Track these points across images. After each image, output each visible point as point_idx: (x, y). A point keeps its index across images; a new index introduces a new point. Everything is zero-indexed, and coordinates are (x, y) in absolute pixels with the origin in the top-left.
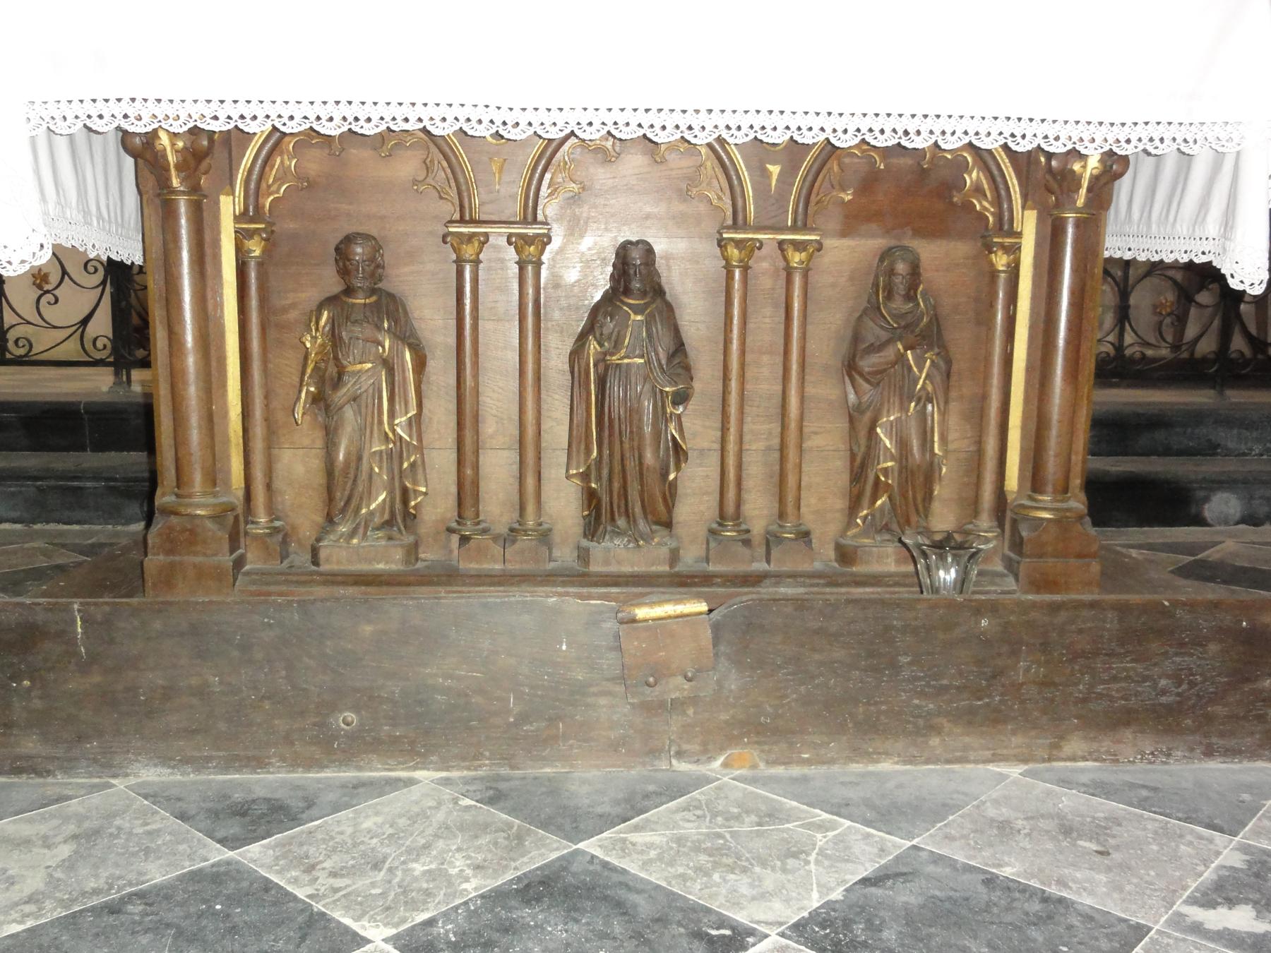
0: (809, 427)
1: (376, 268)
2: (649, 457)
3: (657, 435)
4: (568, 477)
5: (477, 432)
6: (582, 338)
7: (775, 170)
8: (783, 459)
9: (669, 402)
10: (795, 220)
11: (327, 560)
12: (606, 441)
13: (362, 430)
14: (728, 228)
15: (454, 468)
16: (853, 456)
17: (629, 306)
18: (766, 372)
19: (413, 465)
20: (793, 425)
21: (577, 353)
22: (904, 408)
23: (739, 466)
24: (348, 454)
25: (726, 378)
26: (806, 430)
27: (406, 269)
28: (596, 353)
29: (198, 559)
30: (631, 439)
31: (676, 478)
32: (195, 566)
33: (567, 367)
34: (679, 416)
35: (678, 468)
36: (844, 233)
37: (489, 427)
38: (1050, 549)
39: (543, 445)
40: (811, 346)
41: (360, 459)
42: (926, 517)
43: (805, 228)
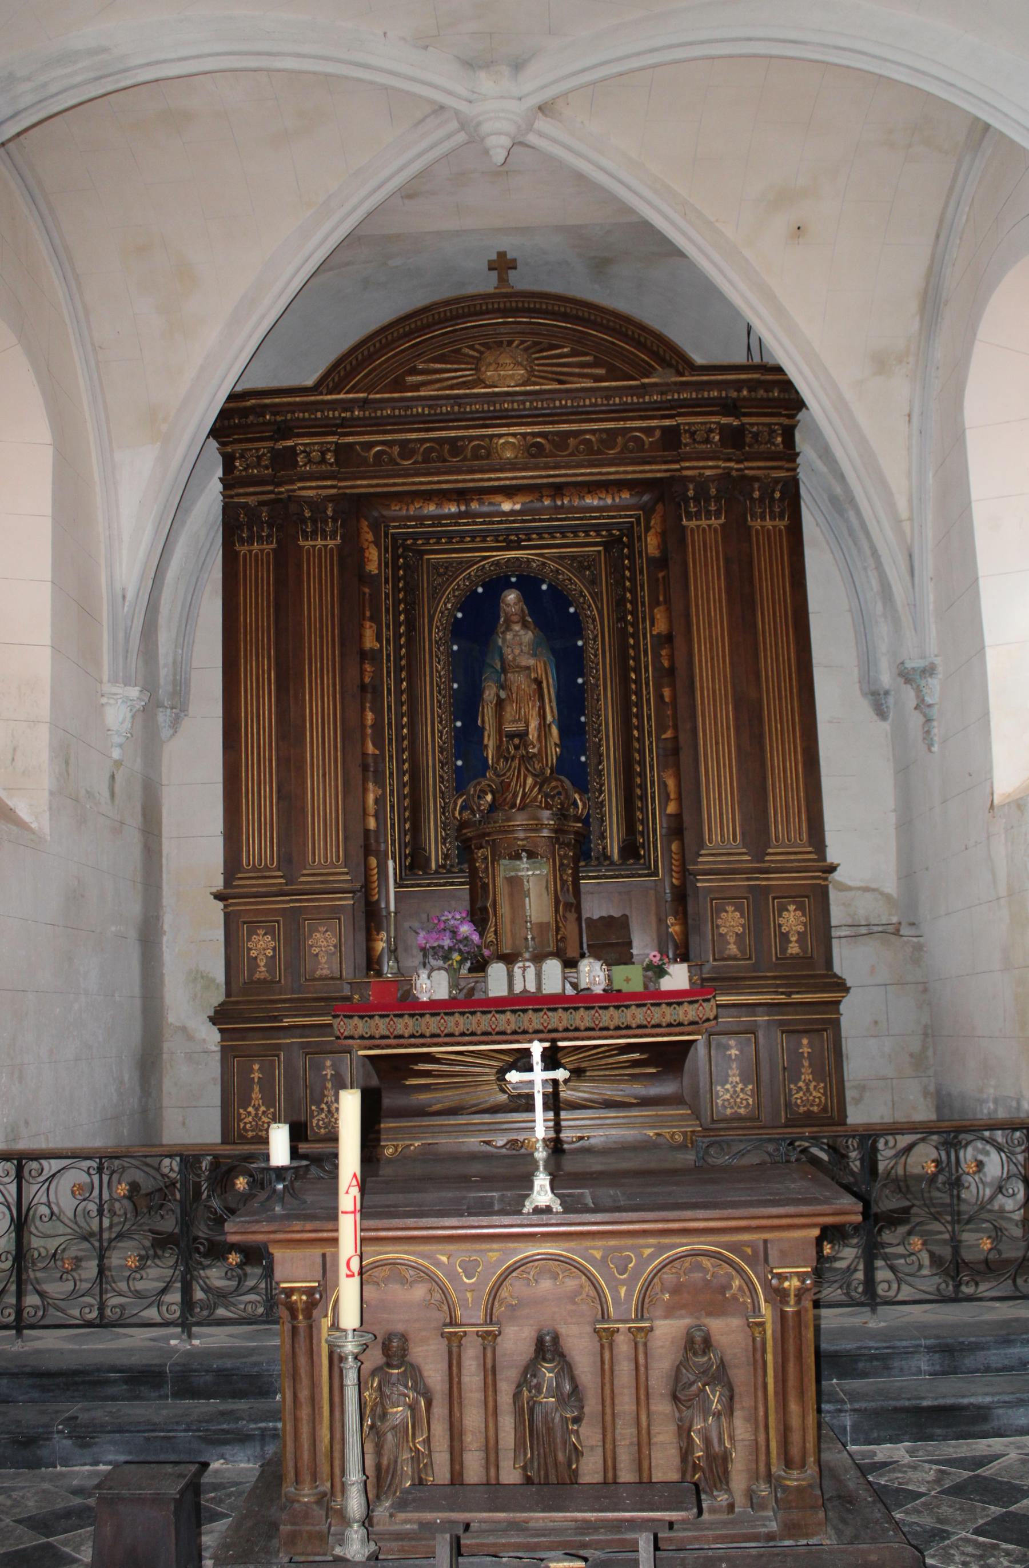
0: (654, 1430)
1: (404, 1351)
2: (561, 1457)
3: (565, 1443)
4: (515, 1468)
5: (461, 1441)
6: (519, 1386)
7: (623, 1291)
8: (639, 1451)
9: (569, 1423)
10: (636, 1315)
11: (378, 1524)
12: (535, 1447)
13: (397, 1446)
14: (599, 1322)
15: (448, 1463)
16: (681, 1448)
17: (546, 1368)
18: (627, 1399)
19: (425, 1465)
20: (644, 1432)
21: (517, 1396)
22: (705, 1420)
23: (614, 1459)
24: (389, 1459)
25: (603, 1406)
26: (652, 1432)
27: (420, 1349)
28: (528, 1397)
29: (309, 1528)
30: (550, 1446)
31: (577, 1467)
32: (307, 1532)
33: (511, 1401)
34: (577, 1431)
35: (578, 1461)
36: (666, 1317)
37: (468, 1438)
38: (794, 1504)
39: (500, 1447)
40: (652, 1382)
41: (396, 1462)
42: (727, 1483)
43: (642, 1319)
